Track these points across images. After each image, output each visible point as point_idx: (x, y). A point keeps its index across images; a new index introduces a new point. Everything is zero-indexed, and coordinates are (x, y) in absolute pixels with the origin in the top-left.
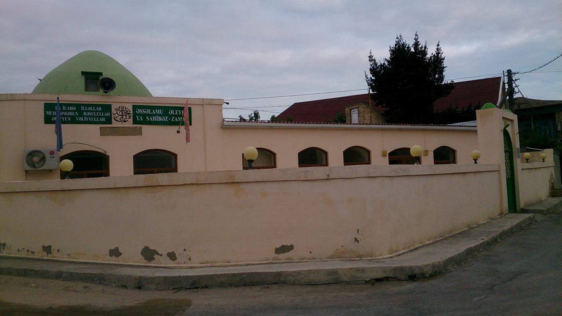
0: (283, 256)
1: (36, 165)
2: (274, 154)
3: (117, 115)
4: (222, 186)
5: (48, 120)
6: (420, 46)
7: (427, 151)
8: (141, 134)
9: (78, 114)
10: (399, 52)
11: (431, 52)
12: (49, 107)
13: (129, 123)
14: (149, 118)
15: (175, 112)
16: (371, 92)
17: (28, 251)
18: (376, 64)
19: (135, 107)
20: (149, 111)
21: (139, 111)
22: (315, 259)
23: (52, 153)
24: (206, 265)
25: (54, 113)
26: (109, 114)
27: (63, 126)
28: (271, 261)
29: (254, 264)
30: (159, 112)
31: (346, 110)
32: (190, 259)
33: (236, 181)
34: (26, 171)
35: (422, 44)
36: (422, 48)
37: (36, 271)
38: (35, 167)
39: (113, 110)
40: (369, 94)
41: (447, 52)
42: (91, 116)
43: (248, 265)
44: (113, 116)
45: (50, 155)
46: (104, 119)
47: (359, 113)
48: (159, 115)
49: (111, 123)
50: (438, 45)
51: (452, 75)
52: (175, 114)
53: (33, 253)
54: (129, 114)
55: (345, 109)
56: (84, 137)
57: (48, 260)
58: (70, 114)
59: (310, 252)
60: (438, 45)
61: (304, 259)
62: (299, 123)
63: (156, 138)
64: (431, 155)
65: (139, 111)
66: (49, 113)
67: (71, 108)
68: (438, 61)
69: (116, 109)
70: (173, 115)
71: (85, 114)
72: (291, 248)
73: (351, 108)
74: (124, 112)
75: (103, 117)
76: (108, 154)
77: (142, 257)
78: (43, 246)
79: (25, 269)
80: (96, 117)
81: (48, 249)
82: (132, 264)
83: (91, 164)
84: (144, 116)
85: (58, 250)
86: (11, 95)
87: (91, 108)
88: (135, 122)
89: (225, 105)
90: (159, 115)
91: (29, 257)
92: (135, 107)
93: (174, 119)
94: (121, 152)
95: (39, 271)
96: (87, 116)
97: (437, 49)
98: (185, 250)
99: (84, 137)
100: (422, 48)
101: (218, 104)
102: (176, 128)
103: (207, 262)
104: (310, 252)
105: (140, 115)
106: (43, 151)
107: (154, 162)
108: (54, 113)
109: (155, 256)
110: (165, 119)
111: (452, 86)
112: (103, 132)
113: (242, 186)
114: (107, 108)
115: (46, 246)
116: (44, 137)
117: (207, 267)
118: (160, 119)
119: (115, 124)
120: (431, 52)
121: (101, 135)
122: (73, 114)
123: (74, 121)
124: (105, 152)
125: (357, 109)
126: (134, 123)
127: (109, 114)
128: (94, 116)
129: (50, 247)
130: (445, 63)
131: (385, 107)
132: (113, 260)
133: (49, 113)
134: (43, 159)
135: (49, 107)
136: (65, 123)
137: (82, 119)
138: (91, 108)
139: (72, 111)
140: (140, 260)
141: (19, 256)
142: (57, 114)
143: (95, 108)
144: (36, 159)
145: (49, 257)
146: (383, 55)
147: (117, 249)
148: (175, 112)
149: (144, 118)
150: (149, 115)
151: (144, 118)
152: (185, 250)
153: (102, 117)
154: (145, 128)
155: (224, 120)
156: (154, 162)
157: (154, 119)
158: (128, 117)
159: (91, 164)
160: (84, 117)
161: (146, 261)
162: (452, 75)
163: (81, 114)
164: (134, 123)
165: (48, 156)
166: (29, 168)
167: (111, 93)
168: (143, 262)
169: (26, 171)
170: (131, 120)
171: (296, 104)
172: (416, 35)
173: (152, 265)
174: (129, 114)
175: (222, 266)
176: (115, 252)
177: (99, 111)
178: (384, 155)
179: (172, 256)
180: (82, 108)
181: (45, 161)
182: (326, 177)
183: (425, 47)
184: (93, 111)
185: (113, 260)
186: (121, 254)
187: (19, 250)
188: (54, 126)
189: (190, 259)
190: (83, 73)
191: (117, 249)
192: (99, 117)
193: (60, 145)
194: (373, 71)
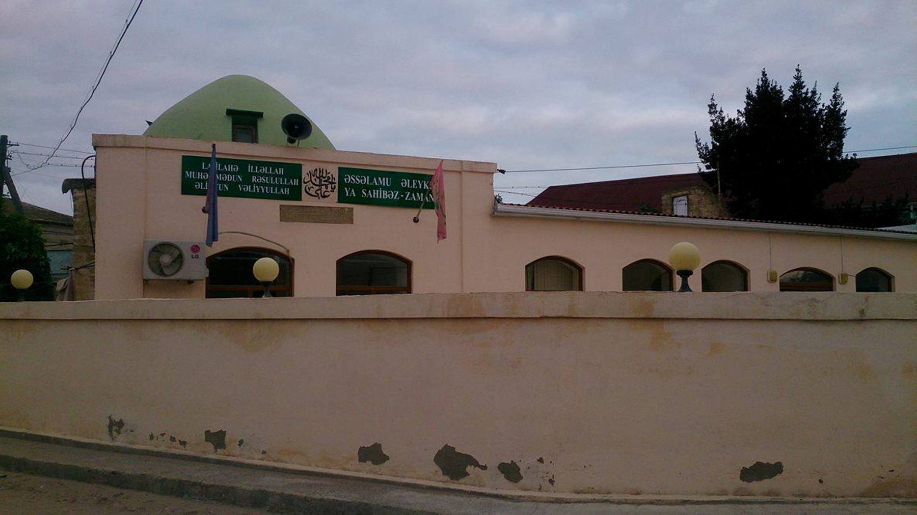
0: (756, 486)
1: (166, 271)
2: (580, 270)
4: (624, 324)
5: (188, 188)
6: (804, 90)
7: (846, 275)
9: (244, 180)
10: (764, 100)
11: (825, 100)
12: (190, 163)
13: (332, 201)
14: (367, 192)
15: (411, 183)
16: (704, 170)
17: (173, 439)
18: (723, 119)
19: (343, 171)
20: (366, 180)
21: (350, 179)
22: (831, 496)
23: (195, 249)
24: (589, 497)
25: (200, 175)
27: (220, 200)
28: (730, 497)
29: (698, 503)
30: (384, 181)
31: (663, 198)
32: (551, 481)
33: (655, 315)
34: (146, 282)
35: (809, 86)
36: (807, 93)
37: (207, 487)
38: (162, 273)
40: (701, 174)
41: (849, 105)
42: (265, 185)
43: (684, 502)
44: (304, 185)
45: (191, 253)
46: (287, 191)
47: (689, 204)
50: (836, 90)
51: (854, 146)
52: (412, 188)
53: (183, 443)
54: (331, 183)
55: (660, 199)
56: (249, 221)
57: (218, 462)
58: (228, 178)
59: (821, 481)
60: (836, 90)
61: (805, 496)
62: (620, 212)
63: (377, 229)
64: (852, 283)
65: (350, 179)
66: (190, 174)
67: (231, 168)
68: (835, 116)
70: (407, 189)
71: (254, 179)
72: (776, 469)
73: (673, 195)
74: (322, 178)
75: (287, 186)
76: (292, 255)
77: (437, 468)
78: (207, 432)
79: (180, 481)
80: (274, 186)
81: (217, 439)
82: (413, 481)
84: (358, 188)
85: (241, 442)
86: (125, 137)
87: (265, 170)
89: (497, 176)
91: (173, 451)
92: (343, 171)
93: (410, 196)
94: (317, 252)
95: (213, 486)
96: (257, 184)
97: (834, 97)
98: (541, 460)
99: (249, 221)
100: (807, 93)
101: (486, 171)
102: (413, 213)
103: (591, 491)
104: (821, 481)
105: (351, 186)
107: (371, 273)
108: (200, 175)
109: (469, 469)
110: (395, 195)
111: (854, 163)
112: (286, 215)
113: (668, 327)
114: (294, 170)
116: (183, 221)
117: (593, 501)
118: (385, 195)
120: (825, 100)
122: (232, 178)
123: (234, 192)
124: (288, 251)
125: (685, 198)
126: (340, 201)
128: (270, 185)
129: (222, 434)
130: (847, 123)
131: (730, 197)
132: (367, 471)
133: (190, 174)
134: (179, 259)
135: (190, 163)
137: (248, 188)
138: (265, 170)
139: (231, 173)
140: (434, 476)
141: (152, 448)
142: (203, 178)
143: (273, 170)
144: (166, 259)
145: (220, 455)
146: (733, 109)
147: (377, 447)
148: (411, 183)
149: (358, 192)
150: (368, 188)
151: (358, 192)
152: (541, 460)
153: (284, 187)
154: (359, 210)
155: (498, 200)
156: (371, 273)
157: (376, 194)
158: (329, 189)
159: (232, 273)
160: (252, 184)
161: (447, 478)
162: (854, 146)
163: (247, 180)
164: (340, 201)
165: (187, 254)
166: (151, 275)
167: (302, 143)
168: (440, 480)
169: (146, 282)
170: (335, 195)
171: (551, 189)
172: (797, 70)
173: (463, 488)
174: (331, 183)
175: (626, 502)
176: (372, 454)
178: (772, 280)
179: (511, 472)
180: (250, 169)
181: (181, 263)
182: (856, 316)
183: (814, 93)
184: (269, 175)
185: (367, 471)
186: (385, 458)
187: (152, 437)
188: (202, 201)
189: (551, 481)
190: (230, 112)
191: (377, 447)
192: (280, 187)
193: (213, 235)
194: (715, 131)
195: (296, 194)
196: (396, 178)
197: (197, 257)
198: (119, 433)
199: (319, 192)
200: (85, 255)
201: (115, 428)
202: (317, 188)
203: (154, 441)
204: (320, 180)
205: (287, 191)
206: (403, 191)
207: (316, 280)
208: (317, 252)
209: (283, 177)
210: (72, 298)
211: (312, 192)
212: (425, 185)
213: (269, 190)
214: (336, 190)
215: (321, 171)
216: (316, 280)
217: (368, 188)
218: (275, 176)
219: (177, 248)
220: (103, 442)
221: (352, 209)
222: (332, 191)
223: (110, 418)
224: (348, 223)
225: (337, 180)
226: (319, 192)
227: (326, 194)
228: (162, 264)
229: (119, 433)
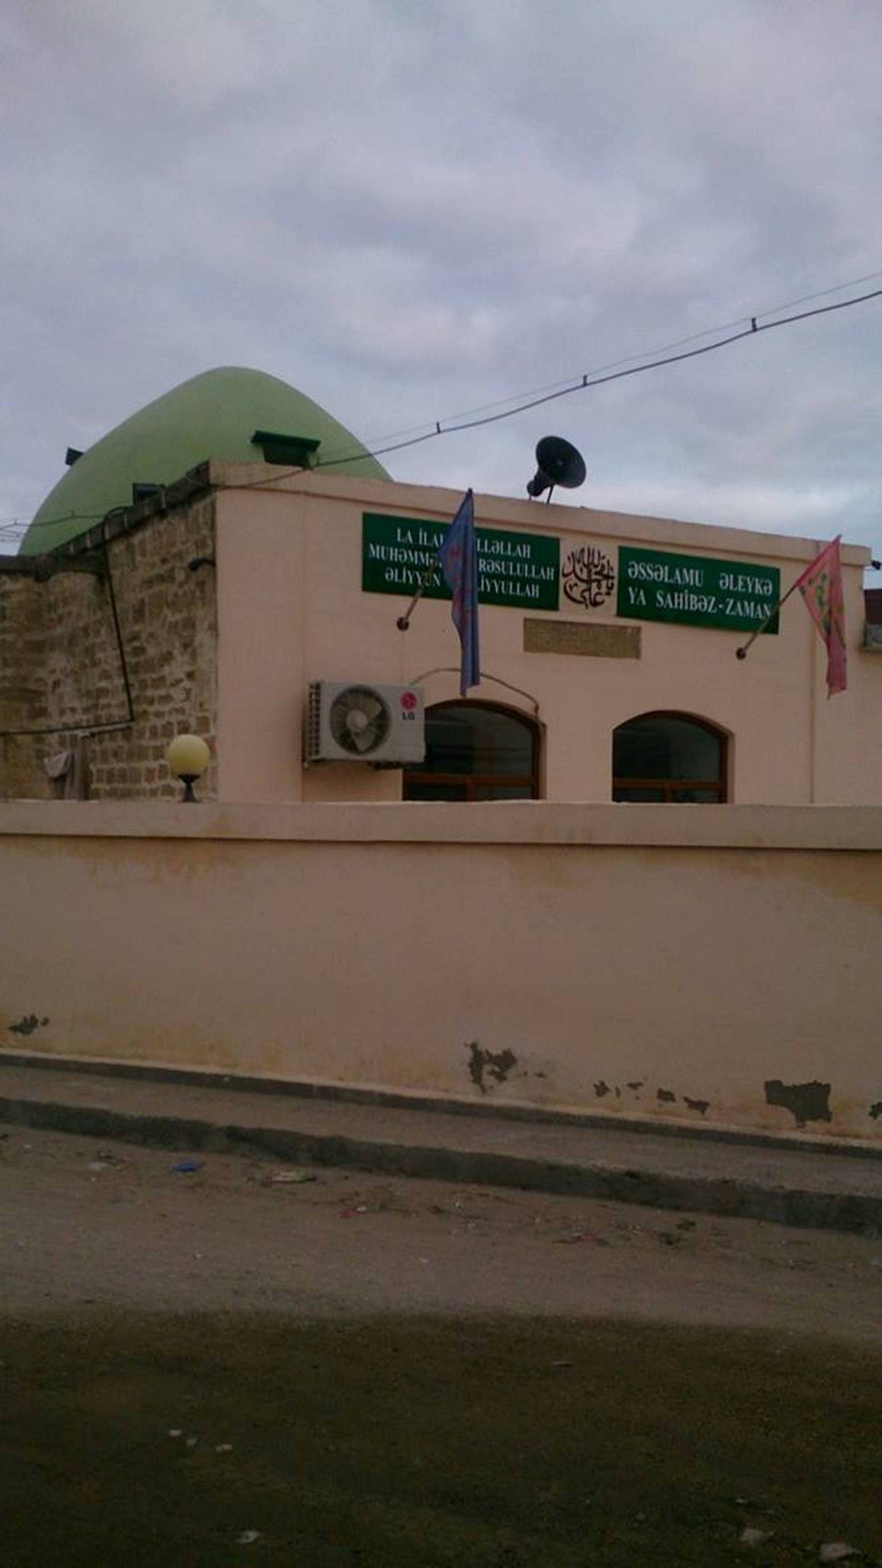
3: (573, 579)
5: (374, 579)
8: (637, 654)
13: (606, 614)
14: (665, 598)
15: (736, 583)
19: (627, 555)
25: (394, 554)
26: (550, 574)
30: (692, 577)
39: (563, 559)
44: (562, 581)
46: (534, 591)
48: (693, 590)
49: (553, 606)
53: (700, 1106)
54: (608, 577)
65: (638, 570)
66: (377, 552)
69: (572, 557)
70: (729, 593)
80: (515, 579)
83: (475, 753)
84: (650, 587)
87: (499, 547)
88: (623, 611)
90: (693, 590)
92: (627, 555)
93: (734, 606)
94: (581, 708)
102: (740, 639)
105: (639, 584)
106: (384, 695)
107: (667, 757)
108: (394, 554)
110: (708, 605)
115: (788, 1082)
118: (694, 603)
119: (568, 612)
121: (527, 648)
124: (537, 708)
126: (621, 613)
127: (550, 574)
133: (377, 552)
134: (381, 724)
136: (489, 598)
138: (499, 547)
145: (814, 1133)
151: (651, 598)
154: (652, 633)
157: (678, 602)
158: (604, 590)
164: (621, 613)
165: (396, 711)
170: (611, 602)
174: (608, 577)
177: (523, 561)
184: (507, 559)
192: (526, 582)
195: (548, 599)
196: (712, 569)
197: (412, 716)
198: (501, 1078)
199: (586, 594)
200: (25, 708)
201: (487, 1068)
202: (583, 586)
203: (609, 1097)
204: (589, 572)
205: (534, 591)
206: (722, 596)
207: (578, 768)
208: (581, 708)
209: (529, 562)
210: (86, 794)
211: (576, 593)
212: (758, 586)
213: (507, 587)
214: (615, 591)
215: (591, 553)
216: (578, 768)
217: (673, 589)
218: (517, 560)
219: (378, 699)
220: (460, 1098)
221: (638, 630)
222: (608, 594)
223: (474, 1047)
224: (630, 657)
225: (615, 573)
226: (586, 594)
227: (599, 599)
228: (338, 734)
229: (501, 1078)
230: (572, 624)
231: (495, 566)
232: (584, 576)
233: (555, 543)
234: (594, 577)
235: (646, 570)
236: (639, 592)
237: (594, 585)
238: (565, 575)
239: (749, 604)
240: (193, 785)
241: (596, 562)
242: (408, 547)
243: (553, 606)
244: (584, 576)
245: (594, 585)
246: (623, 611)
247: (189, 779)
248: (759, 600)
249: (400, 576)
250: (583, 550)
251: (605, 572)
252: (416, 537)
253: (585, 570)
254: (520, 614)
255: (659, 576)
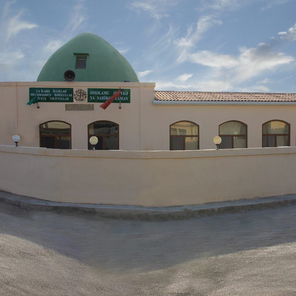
3: (77, 96)
13: (85, 102)
14: (99, 98)
26: (71, 95)
39: (74, 92)
44: (74, 96)
48: (107, 96)
65: (92, 93)
87: (59, 91)
88: (89, 101)
90: (107, 96)
105: (92, 95)
121: (66, 110)
133: (32, 95)
138: (59, 91)
158: (84, 97)
170: (87, 99)
177: (65, 93)
184: (61, 93)
192: (65, 97)
195: (71, 100)
204: (80, 94)
205: (68, 99)
207: (80, 135)
211: (77, 98)
212: (124, 93)
215: (81, 90)
216: (80, 135)
218: (63, 93)
221: (93, 105)
225: (87, 94)
227: (83, 99)
230: (77, 104)
231: (58, 95)
232: (79, 95)
233: (72, 89)
234: (82, 95)
235: (94, 92)
236: (93, 97)
237: (82, 97)
238: (75, 95)
239: (121, 97)
240: (17, 144)
241: (82, 92)
242: (39, 93)
243: (72, 101)
244: (79, 95)
245: (82, 97)
246: (89, 101)
247: (16, 143)
248: (125, 96)
249: (55, 99)
250: (79, 90)
251: (84, 94)
252: (40, 91)
253: (79, 94)
254: (64, 104)
255: (98, 93)
